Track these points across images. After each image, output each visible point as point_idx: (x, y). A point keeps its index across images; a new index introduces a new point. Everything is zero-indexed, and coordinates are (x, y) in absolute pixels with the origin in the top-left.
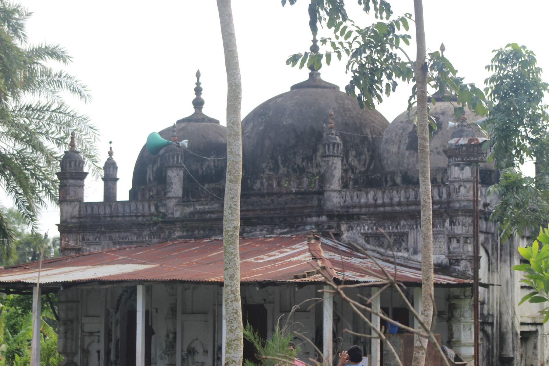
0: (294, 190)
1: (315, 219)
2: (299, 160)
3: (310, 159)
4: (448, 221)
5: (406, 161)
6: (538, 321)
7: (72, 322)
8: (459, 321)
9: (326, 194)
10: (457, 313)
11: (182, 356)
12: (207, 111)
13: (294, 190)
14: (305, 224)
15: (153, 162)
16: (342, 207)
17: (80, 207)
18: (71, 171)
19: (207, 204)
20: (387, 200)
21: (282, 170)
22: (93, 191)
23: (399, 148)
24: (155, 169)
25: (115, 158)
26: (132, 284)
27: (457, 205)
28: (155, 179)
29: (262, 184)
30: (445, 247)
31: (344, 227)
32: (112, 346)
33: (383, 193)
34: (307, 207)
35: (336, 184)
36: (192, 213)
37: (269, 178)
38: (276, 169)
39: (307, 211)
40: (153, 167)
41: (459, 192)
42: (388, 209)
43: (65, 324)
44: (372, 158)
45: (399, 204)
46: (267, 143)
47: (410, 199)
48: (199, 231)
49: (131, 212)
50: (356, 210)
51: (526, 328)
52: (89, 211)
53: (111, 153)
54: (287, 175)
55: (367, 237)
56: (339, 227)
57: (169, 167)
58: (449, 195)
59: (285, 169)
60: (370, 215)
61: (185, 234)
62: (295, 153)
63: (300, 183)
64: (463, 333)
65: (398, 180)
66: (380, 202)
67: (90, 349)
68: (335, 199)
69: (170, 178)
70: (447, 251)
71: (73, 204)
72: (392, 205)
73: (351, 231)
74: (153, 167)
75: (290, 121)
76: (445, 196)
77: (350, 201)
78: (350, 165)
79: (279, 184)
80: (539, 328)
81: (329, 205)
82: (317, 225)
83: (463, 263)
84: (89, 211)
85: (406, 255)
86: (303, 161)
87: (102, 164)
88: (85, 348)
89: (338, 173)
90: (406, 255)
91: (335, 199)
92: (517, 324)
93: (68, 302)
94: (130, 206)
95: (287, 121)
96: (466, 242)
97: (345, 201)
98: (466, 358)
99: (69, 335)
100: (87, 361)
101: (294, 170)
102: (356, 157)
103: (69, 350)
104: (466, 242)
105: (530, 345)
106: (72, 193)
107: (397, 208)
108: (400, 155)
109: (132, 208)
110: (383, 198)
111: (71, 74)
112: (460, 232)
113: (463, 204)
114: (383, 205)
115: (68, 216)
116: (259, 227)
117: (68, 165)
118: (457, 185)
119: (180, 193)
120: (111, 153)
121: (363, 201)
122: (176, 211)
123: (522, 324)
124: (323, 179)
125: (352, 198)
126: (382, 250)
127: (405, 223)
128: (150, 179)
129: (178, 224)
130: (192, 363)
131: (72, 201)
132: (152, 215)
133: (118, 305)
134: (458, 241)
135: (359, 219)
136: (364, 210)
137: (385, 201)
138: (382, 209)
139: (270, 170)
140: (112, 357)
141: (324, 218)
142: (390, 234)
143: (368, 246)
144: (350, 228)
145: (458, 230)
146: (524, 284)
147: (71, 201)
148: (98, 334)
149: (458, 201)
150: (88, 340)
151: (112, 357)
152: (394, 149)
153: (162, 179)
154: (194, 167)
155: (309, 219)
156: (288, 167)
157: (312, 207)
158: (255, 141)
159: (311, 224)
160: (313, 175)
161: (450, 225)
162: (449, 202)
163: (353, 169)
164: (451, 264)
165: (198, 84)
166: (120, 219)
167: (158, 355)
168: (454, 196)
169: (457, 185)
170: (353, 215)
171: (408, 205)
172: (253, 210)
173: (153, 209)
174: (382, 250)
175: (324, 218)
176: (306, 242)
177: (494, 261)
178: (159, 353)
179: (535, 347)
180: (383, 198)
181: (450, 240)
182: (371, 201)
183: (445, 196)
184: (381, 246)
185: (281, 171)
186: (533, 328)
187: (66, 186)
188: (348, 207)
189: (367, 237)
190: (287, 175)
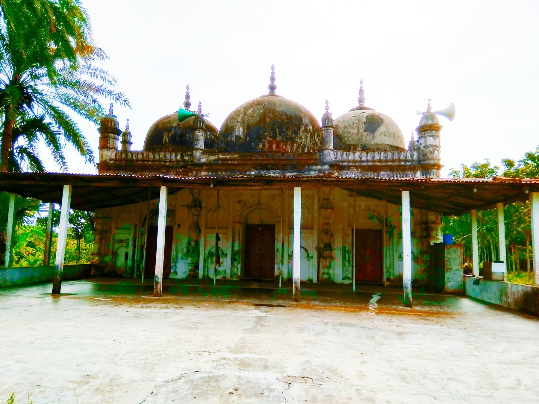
2: (290, 133)
3: (296, 133)
5: (364, 138)
7: (106, 232)
11: (204, 258)
15: (158, 136)
16: (333, 161)
17: (116, 154)
19: (228, 155)
20: (369, 158)
21: (279, 138)
23: (358, 130)
24: (170, 135)
28: (170, 142)
29: (264, 146)
34: (311, 159)
36: (217, 160)
37: (269, 142)
40: (168, 134)
41: (434, 153)
43: (100, 234)
45: (380, 161)
47: (388, 158)
48: (222, 172)
49: (160, 158)
52: (124, 156)
57: (198, 128)
59: (281, 138)
61: (210, 173)
62: (287, 128)
67: (118, 252)
69: (198, 136)
71: (112, 150)
72: (374, 161)
74: (168, 134)
77: (340, 158)
79: (278, 146)
84: (124, 156)
86: (292, 134)
88: (115, 251)
93: (103, 218)
94: (160, 155)
97: (336, 158)
99: (103, 242)
100: (115, 260)
103: (102, 252)
106: (111, 143)
108: (360, 135)
109: (161, 156)
110: (367, 157)
115: (108, 158)
117: (109, 123)
118: (431, 149)
122: (203, 158)
125: (342, 156)
127: (384, 173)
128: (166, 141)
130: (211, 263)
131: (112, 148)
135: (348, 169)
137: (368, 158)
138: (365, 164)
139: (270, 137)
141: (327, 167)
147: (111, 148)
148: (127, 241)
149: (433, 159)
150: (117, 246)
152: (355, 131)
155: (314, 167)
156: (283, 136)
158: (258, 119)
159: (315, 170)
166: (150, 163)
167: (179, 257)
170: (345, 166)
171: (386, 161)
172: (268, 160)
173: (179, 157)
175: (327, 167)
180: (367, 157)
185: (278, 139)
187: (107, 137)
188: (339, 161)
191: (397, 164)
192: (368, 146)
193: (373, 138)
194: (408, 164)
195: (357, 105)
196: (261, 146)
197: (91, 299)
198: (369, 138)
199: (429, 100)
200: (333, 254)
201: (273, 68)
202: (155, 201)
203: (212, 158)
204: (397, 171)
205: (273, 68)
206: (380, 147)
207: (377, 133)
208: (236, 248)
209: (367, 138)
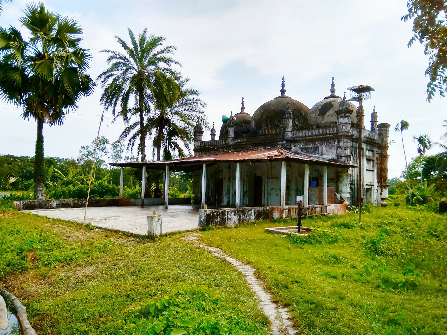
0: (274, 133)
1: (281, 143)
4: (337, 141)
6: (372, 184)
8: (342, 182)
9: (286, 133)
10: (340, 179)
12: (246, 111)
13: (274, 133)
14: (278, 145)
16: (292, 138)
18: (198, 131)
20: (310, 134)
21: (270, 126)
22: (206, 137)
25: (215, 128)
26: (200, 164)
27: (341, 134)
29: (262, 131)
30: (335, 152)
31: (292, 146)
32: (210, 190)
33: (309, 131)
34: (278, 138)
35: (290, 129)
36: (236, 143)
37: (265, 129)
38: (267, 126)
39: (278, 140)
42: (311, 138)
44: (304, 122)
45: (316, 135)
46: (264, 116)
50: (298, 139)
51: (368, 187)
53: (213, 126)
54: (271, 128)
55: (302, 149)
56: (290, 145)
58: (337, 130)
60: (303, 140)
63: (276, 130)
64: (343, 188)
65: (315, 127)
66: (307, 135)
68: (289, 135)
70: (336, 154)
72: (312, 136)
73: (291, 323)
75: (273, 108)
76: (335, 131)
78: (295, 124)
79: (268, 131)
80: (372, 187)
81: (287, 137)
82: (282, 145)
83: (343, 158)
85: (318, 156)
87: (211, 129)
89: (291, 124)
90: (318, 156)
91: (289, 135)
92: (365, 185)
95: (271, 108)
96: (345, 149)
98: (345, 198)
101: (274, 126)
102: (298, 121)
104: (345, 149)
105: (369, 193)
107: (315, 137)
111: (201, 99)
112: (342, 145)
113: (344, 133)
114: (309, 136)
116: (260, 147)
118: (341, 126)
119: (233, 136)
120: (213, 126)
121: (300, 135)
123: (366, 185)
124: (285, 128)
125: (296, 134)
126: (308, 154)
129: (232, 147)
132: (223, 144)
133: (212, 177)
134: (342, 149)
135: (299, 142)
136: (301, 139)
140: (210, 195)
141: (285, 142)
142: (311, 148)
143: (302, 153)
144: (295, 146)
145: (342, 144)
146: (367, 169)
147: (198, 141)
149: (342, 132)
151: (210, 195)
152: (313, 116)
153: (228, 132)
154: (240, 128)
157: (280, 138)
159: (279, 145)
160: (281, 128)
161: (338, 142)
162: (337, 133)
163: (296, 125)
164: (338, 158)
165: (243, 102)
168: (340, 130)
169: (341, 126)
170: (296, 141)
174: (308, 154)
175: (285, 142)
176: (277, 151)
177: (355, 159)
178: (225, 193)
179: (371, 195)
181: (337, 149)
182: (304, 135)
183: (335, 131)
184: (308, 152)
185: (269, 126)
186: (370, 187)
188: (294, 138)
189: (302, 149)
190: (271, 128)
191: (325, 136)
192: (319, 125)
193: (323, 119)
194: (331, 136)
195: (329, 94)
196: (261, 132)
197: (193, 213)
198: (321, 119)
199: (345, 92)
200: (290, 193)
201: (283, 79)
202: (161, 172)
203: (235, 142)
204: (325, 140)
205: (283, 79)
206: (327, 124)
207: (326, 116)
208: (245, 190)
209: (320, 120)
